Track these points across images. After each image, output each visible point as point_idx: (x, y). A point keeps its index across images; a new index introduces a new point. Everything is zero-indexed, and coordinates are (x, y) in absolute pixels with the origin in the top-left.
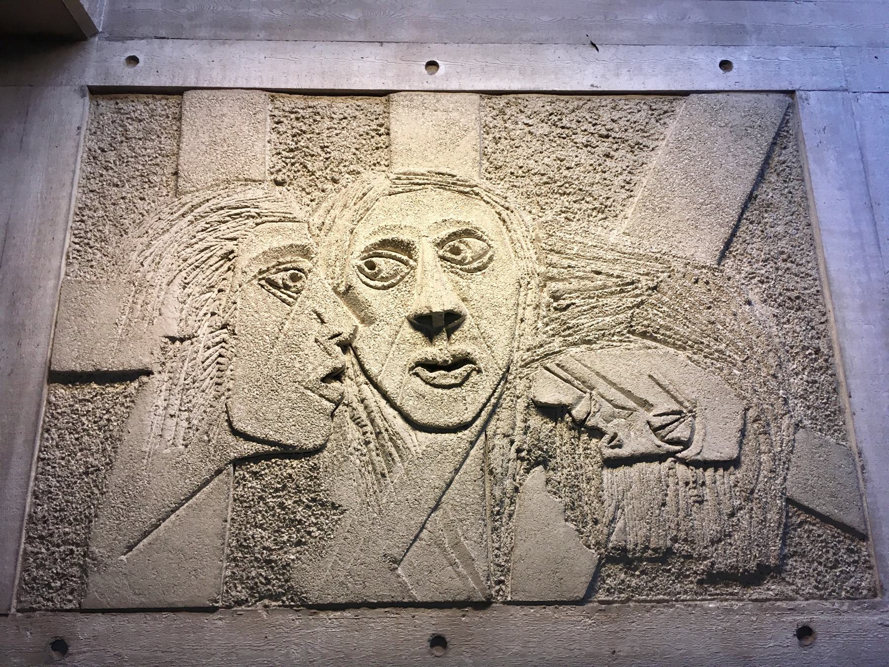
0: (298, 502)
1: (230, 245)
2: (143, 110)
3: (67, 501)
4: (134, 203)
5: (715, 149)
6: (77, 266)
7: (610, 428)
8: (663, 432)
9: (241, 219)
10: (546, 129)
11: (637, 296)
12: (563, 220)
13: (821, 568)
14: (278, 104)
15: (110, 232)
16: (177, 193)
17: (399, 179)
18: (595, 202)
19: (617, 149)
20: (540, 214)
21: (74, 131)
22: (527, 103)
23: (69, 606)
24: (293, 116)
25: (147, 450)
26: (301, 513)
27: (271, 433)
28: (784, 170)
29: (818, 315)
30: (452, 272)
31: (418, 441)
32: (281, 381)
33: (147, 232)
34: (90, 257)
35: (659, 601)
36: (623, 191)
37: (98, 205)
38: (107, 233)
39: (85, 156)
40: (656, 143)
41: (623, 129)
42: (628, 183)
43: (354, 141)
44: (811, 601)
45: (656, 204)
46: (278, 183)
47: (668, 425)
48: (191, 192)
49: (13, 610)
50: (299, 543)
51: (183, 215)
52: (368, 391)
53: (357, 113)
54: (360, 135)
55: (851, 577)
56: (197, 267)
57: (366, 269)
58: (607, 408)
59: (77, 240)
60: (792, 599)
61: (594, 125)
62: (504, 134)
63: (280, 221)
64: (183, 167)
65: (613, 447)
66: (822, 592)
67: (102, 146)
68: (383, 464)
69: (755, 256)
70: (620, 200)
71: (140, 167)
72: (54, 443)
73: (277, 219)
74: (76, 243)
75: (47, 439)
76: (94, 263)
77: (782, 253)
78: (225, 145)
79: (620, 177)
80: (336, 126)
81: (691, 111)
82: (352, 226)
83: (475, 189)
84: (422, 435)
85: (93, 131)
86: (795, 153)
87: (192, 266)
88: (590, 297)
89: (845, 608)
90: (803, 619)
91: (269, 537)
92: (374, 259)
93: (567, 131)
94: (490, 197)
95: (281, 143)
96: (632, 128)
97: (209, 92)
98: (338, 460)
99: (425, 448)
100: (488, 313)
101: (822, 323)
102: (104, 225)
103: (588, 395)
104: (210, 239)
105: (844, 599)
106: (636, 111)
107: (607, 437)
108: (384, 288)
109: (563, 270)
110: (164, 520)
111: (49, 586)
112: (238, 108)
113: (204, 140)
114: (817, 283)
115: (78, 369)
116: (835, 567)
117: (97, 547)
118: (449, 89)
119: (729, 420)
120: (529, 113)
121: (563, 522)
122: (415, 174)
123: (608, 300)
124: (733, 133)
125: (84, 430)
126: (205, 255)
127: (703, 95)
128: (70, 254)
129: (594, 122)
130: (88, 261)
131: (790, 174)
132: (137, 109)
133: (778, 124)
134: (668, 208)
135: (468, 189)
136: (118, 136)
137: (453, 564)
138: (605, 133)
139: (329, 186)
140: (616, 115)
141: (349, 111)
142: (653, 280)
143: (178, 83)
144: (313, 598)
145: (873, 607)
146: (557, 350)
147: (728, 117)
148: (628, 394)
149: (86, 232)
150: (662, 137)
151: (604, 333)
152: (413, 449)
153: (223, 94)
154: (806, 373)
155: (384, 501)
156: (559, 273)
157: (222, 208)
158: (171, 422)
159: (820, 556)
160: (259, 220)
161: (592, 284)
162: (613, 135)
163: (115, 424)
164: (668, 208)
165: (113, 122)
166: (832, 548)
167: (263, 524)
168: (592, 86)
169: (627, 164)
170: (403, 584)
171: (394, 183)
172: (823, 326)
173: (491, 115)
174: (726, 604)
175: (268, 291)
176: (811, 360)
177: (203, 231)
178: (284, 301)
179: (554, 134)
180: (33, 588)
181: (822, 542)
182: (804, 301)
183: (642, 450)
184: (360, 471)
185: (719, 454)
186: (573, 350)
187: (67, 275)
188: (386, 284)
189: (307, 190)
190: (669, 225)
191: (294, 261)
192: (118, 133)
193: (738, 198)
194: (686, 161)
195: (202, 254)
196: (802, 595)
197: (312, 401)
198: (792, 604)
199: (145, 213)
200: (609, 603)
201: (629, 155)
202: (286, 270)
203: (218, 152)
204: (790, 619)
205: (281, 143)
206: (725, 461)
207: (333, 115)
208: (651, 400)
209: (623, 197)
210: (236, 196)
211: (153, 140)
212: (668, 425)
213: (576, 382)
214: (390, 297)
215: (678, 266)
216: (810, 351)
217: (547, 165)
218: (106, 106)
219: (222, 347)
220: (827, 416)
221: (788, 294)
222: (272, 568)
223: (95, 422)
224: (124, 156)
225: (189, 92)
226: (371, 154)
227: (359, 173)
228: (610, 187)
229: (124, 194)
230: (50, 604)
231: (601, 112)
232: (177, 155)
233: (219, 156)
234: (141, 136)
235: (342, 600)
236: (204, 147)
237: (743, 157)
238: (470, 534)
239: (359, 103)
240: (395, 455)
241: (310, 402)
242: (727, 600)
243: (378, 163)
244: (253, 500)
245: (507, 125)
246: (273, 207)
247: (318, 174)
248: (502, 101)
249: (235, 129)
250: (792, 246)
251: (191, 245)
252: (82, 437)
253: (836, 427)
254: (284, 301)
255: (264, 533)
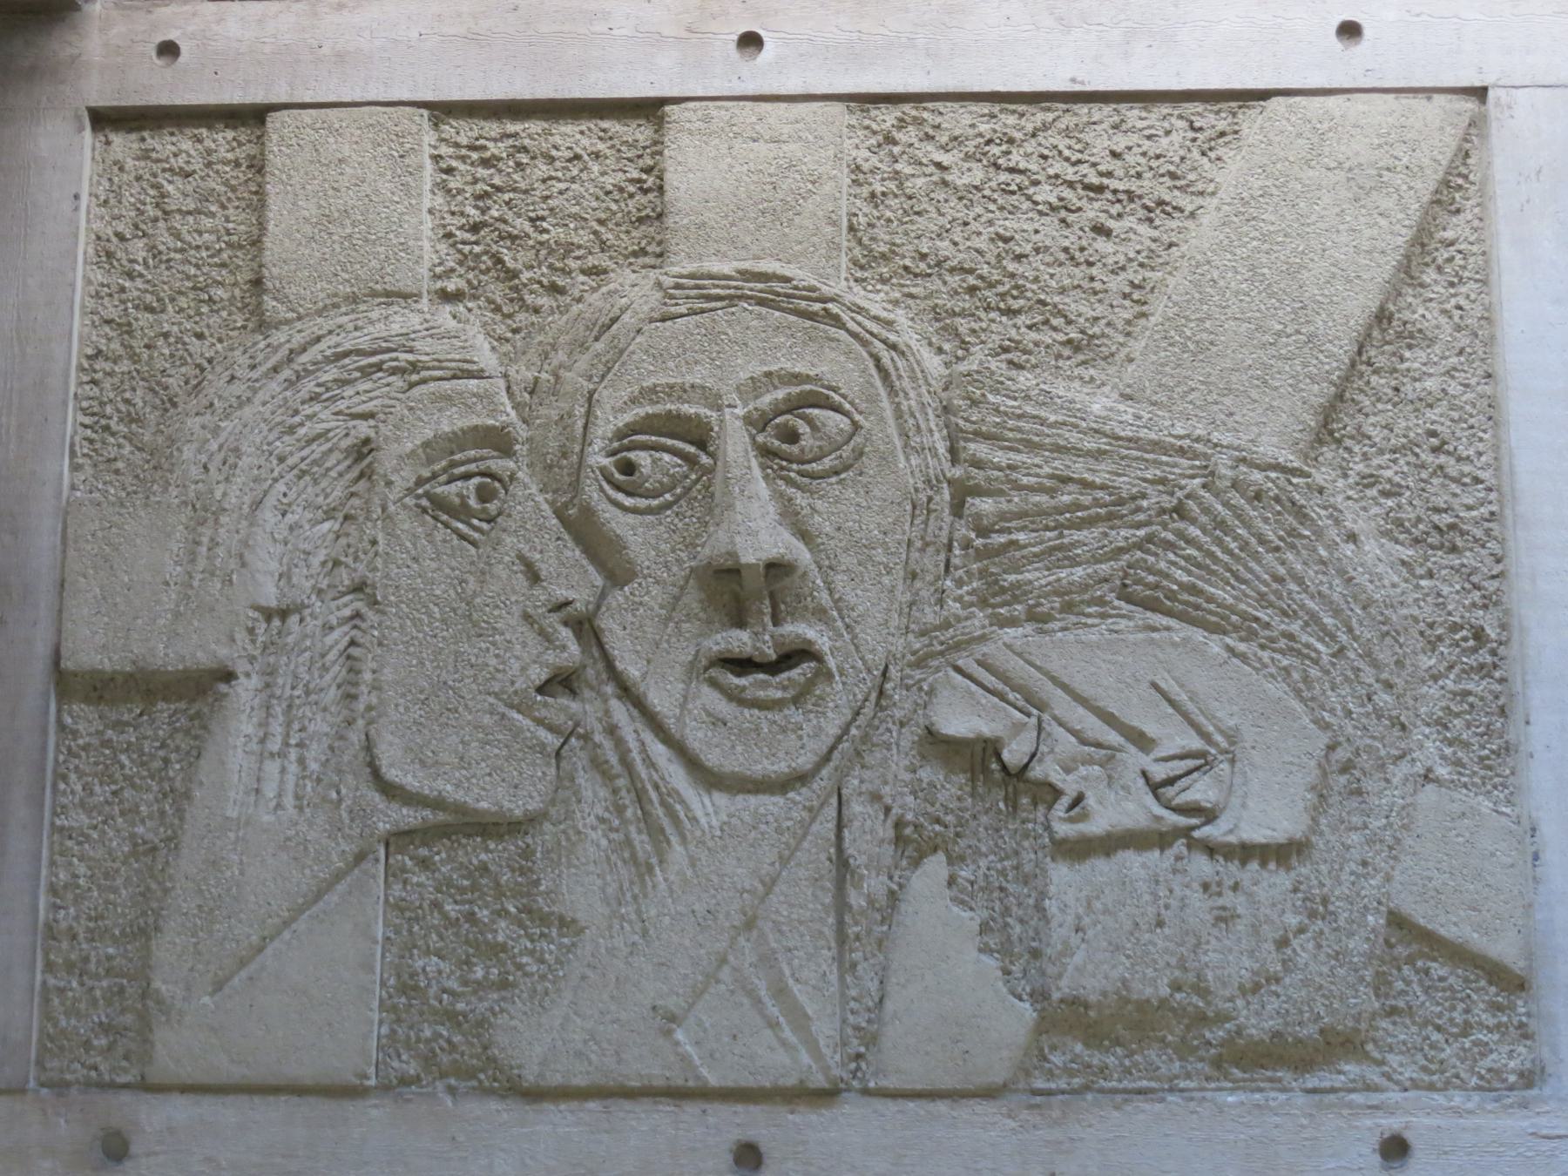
0: (502, 913)
1: (364, 429)
2: (192, 152)
3: (107, 902)
4: (185, 344)
5: (1314, 218)
6: (89, 470)
7: (1069, 785)
8: (1169, 792)
9: (380, 374)
10: (977, 174)
11: (1139, 526)
12: (1004, 366)
13: (1436, 1036)
14: (446, 131)
15: (145, 403)
16: (263, 325)
17: (678, 286)
18: (1069, 329)
19: (1120, 215)
20: (960, 353)
21: (67, 206)
22: (938, 120)
23: (122, 1079)
24: (475, 156)
25: (235, 815)
26: (503, 931)
27: (449, 787)
28: (1450, 260)
29: (1489, 560)
30: (782, 478)
31: (707, 808)
32: (464, 692)
33: (212, 405)
34: (112, 452)
35: (1140, 1092)
36: (1127, 303)
37: (121, 351)
38: (141, 404)
39: (91, 251)
40: (1199, 201)
41: (1132, 172)
42: (1139, 287)
43: (595, 204)
44: (1411, 1094)
45: (1189, 333)
46: (446, 297)
47: (1180, 777)
48: (287, 322)
49: (32, 1084)
50: (504, 985)
51: (275, 369)
52: (620, 712)
53: (601, 146)
54: (608, 193)
55: (1491, 1051)
56: (304, 473)
57: (617, 476)
58: (1067, 743)
59: (87, 420)
60: (1377, 1089)
61: (1074, 164)
62: (892, 185)
63: (454, 377)
64: (272, 273)
65: (1071, 820)
66: (1435, 1078)
67: (120, 229)
68: (649, 848)
69: (1377, 440)
70: (1120, 325)
71: (193, 271)
72: (76, 801)
73: (449, 373)
74: (86, 426)
75: (64, 792)
76: (120, 465)
77: (1433, 434)
78: (348, 222)
79: (1123, 275)
80: (560, 174)
81: (1271, 135)
82: (591, 387)
83: (830, 306)
84: (721, 799)
85: (102, 198)
86: (1476, 223)
87: (295, 471)
88: (1047, 528)
89: (1470, 1105)
90: (1392, 1124)
91: (452, 972)
92: (632, 455)
93: (1018, 178)
94: (859, 324)
95: (453, 213)
96: (1151, 168)
97: (313, 112)
98: (568, 839)
99: (725, 818)
100: (848, 561)
101: (1493, 577)
102: (134, 390)
103: (1034, 720)
104: (326, 418)
105: (1474, 1089)
106: (1161, 133)
107: (1065, 801)
108: (649, 511)
109: (996, 473)
110: (272, 939)
111: (87, 1045)
112: (370, 146)
113: (306, 213)
114: (1493, 496)
115: (107, 666)
116: (1465, 1034)
117: (164, 982)
118: (783, 91)
119: (1294, 769)
120: (944, 140)
121: (975, 954)
122: (711, 277)
123: (1077, 535)
124: (1352, 183)
125: (125, 778)
126: (318, 449)
127: (1298, 99)
128: (77, 448)
129: (1074, 159)
130: (109, 461)
131: (1464, 268)
132: (181, 151)
133: (1444, 163)
134: (1212, 343)
135: (817, 306)
136: (149, 207)
137: (773, 1025)
138: (1094, 180)
139: (545, 301)
140: (1120, 142)
141: (585, 142)
142: (1172, 494)
143: (256, 96)
144: (530, 1077)
145: (1524, 1105)
146: (978, 633)
147: (1343, 148)
148: (1109, 719)
149: (102, 404)
150: (1211, 188)
151: (1071, 603)
152: (703, 821)
153: (342, 115)
154: (1452, 676)
155: (653, 912)
156: (988, 479)
157: (346, 354)
158: (272, 767)
159: (1440, 1016)
160: (415, 377)
161: (1053, 502)
162: (1113, 184)
163: (178, 767)
164: (1212, 343)
165: (139, 178)
166: (1462, 1000)
167: (441, 949)
168: (1073, 80)
169: (1138, 247)
170: (685, 1059)
171: (672, 297)
172: (1495, 584)
173: (868, 143)
174: (1257, 1096)
175: (435, 518)
176: (1464, 650)
177: (311, 399)
178: (462, 537)
179: (993, 184)
180: (62, 1048)
181: (1444, 990)
182: (1463, 534)
183: (1127, 823)
184: (608, 859)
185: (1269, 833)
186: (1010, 633)
187: (73, 487)
188: (655, 502)
189: (505, 310)
190: (1212, 379)
191: (482, 459)
192: (148, 200)
193: (1352, 322)
194: (1255, 243)
195: (314, 446)
196: (1397, 1083)
197: (521, 730)
198: (1375, 1098)
199: (206, 364)
200: (1049, 1093)
201: (1143, 229)
202: (467, 476)
203: (335, 237)
204: (1369, 1123)
205: (453, 213)
206: (1280, 846)
207: (554, 153)
208: (1150, 729)
209: (1126, 316)
210: (371, 329)
211: (212, 215)
212: (1180, 777)
213: (1011, 696)
214: (662, 528)
215: (1223, 465)
216: (1464, 633)
217: (977, 251)
218: (122, 144)
219: (355, 627)
220: (1482, 759)
221: (1436, 518)
222: (459, 1025)
223: (143, 764)
224: (162, 248)
225: (278, 114)
226: (628, 232)
227: (605, 272)
228: (1101, 296)
229: (166, 327)
230: (93, 1074)
231: (1087, 137)
232: (257, 243)
233: (337, 246)
234: (192, 207)
235: (580, 1081)
236: (308, 229)
237: (1368, 233)
238: (805, 974)
239: (605, 124)
240: (669, 830)
241: (516, 732)
242: (1261, 1090)
243: (642, 249)
244: (420, 907)
245: (898, 167)
246: (441, 349)
247: (526, 276)
248: (887, 117)
249: (366, 188)
250: (1452, 420)
251: (291, 430)
252: (122, 789)
253: (1496, 780)
254: (462, 537)
255: (442, 965)
